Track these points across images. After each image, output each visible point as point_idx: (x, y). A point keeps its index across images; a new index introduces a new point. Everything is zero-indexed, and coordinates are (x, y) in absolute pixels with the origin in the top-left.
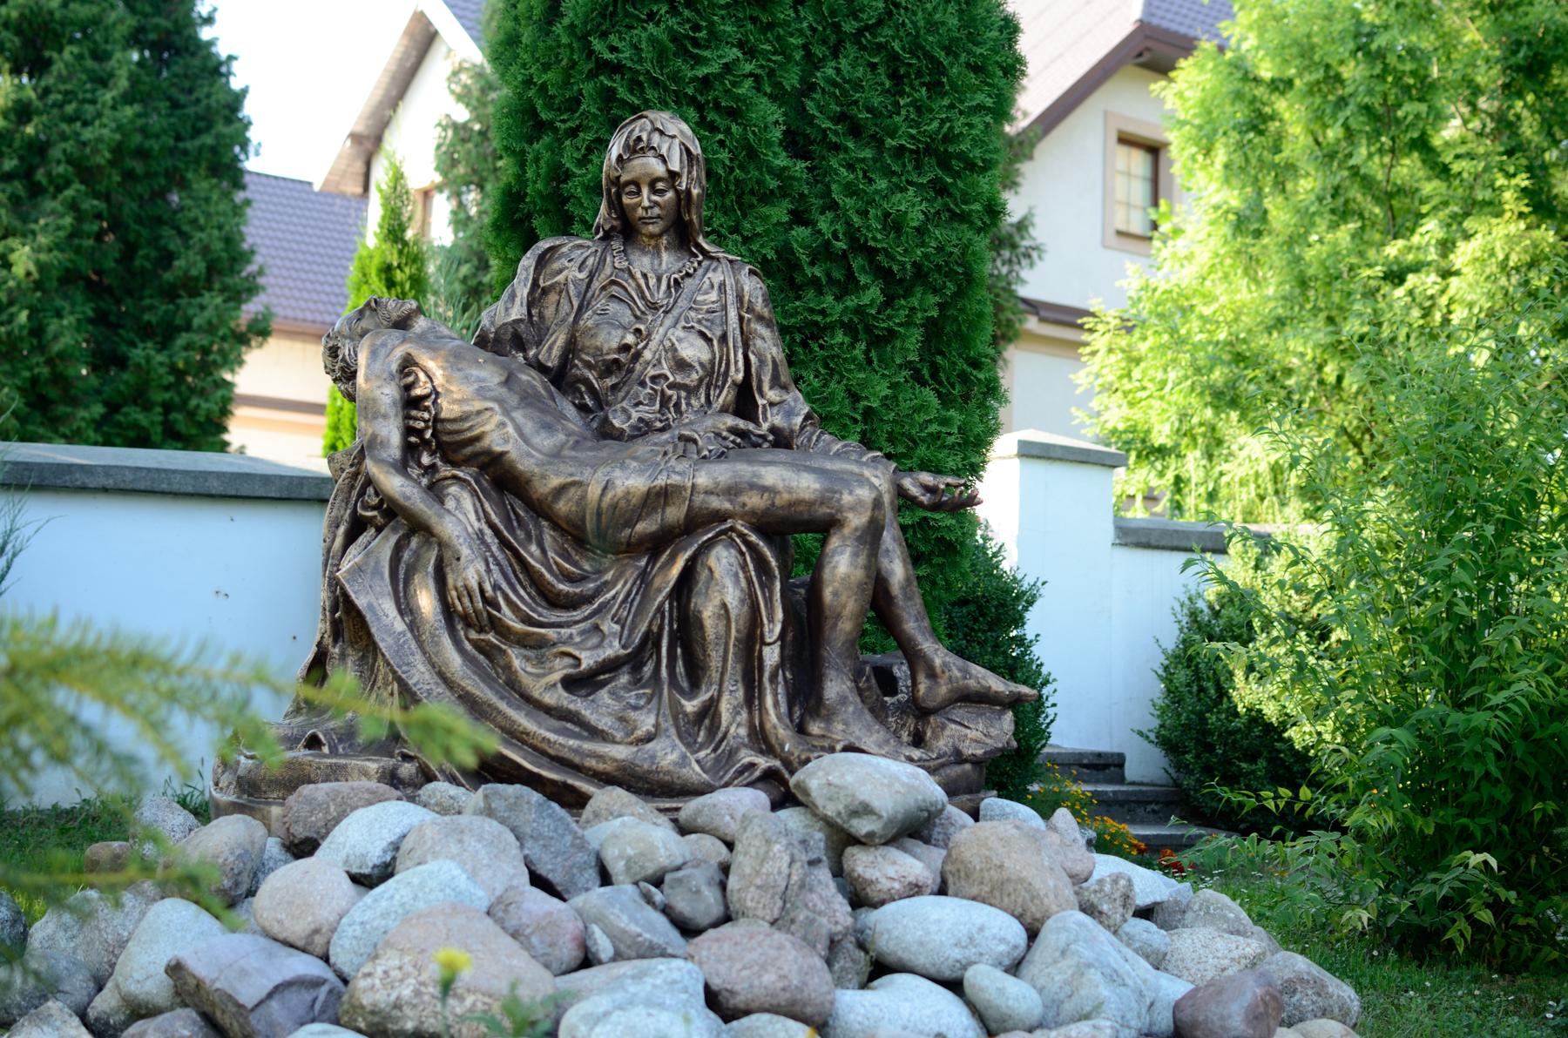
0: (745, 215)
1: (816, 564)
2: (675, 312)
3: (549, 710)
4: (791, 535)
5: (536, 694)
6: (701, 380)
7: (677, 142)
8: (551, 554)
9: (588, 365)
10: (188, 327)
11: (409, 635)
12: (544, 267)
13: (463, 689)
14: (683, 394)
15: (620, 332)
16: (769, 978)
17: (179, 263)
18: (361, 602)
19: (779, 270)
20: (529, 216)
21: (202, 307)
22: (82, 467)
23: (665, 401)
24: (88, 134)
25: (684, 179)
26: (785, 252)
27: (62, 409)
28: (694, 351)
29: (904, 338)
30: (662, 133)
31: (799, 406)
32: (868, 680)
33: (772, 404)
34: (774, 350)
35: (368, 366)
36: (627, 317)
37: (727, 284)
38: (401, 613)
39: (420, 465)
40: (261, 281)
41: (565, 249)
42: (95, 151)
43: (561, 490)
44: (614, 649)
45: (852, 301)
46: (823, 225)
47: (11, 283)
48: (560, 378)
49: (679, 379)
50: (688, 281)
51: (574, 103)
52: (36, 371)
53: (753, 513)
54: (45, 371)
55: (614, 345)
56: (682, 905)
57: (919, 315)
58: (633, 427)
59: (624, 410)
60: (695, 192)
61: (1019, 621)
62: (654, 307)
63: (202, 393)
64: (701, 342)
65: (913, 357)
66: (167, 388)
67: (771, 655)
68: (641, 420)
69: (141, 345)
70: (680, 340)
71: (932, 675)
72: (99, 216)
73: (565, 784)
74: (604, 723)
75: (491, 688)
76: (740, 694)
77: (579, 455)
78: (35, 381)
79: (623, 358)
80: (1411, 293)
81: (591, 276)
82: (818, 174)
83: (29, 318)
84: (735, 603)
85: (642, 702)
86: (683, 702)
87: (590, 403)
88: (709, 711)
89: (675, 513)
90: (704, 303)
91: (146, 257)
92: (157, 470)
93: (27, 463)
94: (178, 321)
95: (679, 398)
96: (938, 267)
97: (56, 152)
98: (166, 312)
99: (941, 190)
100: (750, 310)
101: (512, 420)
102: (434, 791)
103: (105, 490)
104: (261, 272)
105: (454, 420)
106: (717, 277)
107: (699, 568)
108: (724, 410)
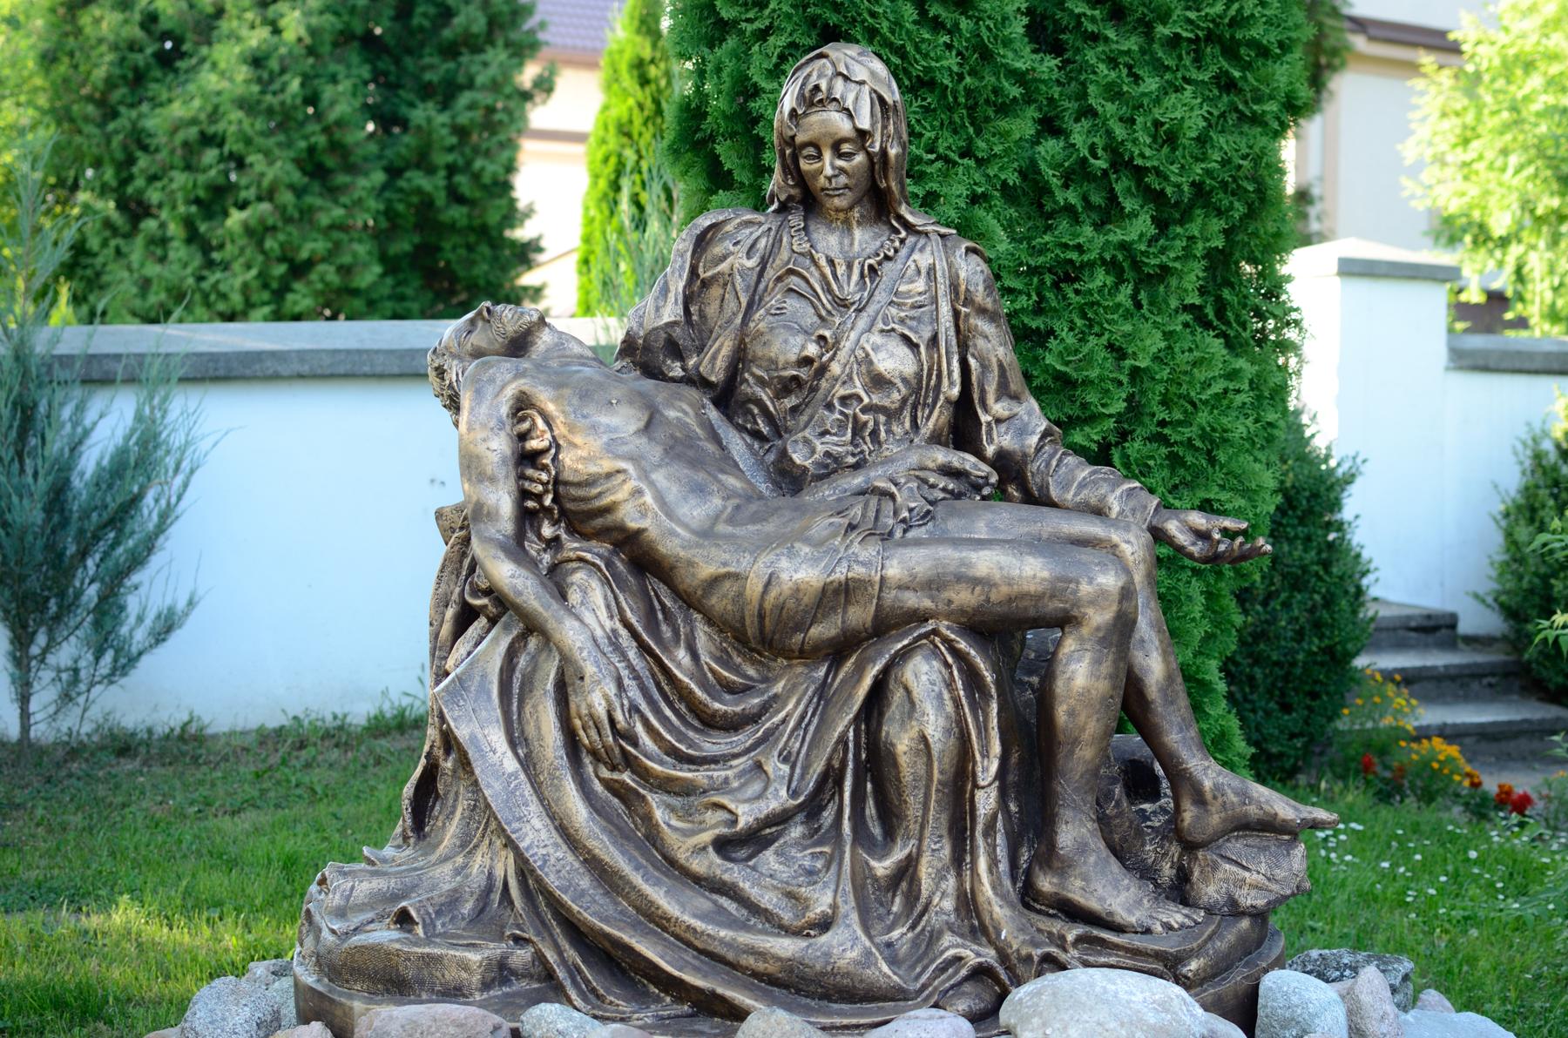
0: (978, 132)
1: (1047, 666)
2: (871, 309)
3: (698, 880)
4: (1010, 639)
5: (682, 856)
6: (904, 401)
7: (866, 89)
8: (705, 658)
9: (761, 382)
10: (470, 85)
11: (522, 776)
12: (704, 250)
13: (589, 851)
14: (882, 418)
15: (800, 339)
17: (459, 21)
18: (462, 732)
19: (1025, 194)
20: (712, 138)
21: (485, 64)
22: (273, 354)
23: (858, 428)
25: (878, 137)
26: (1030, 172)
27: (341, 179)
28: (894, 361)
29: (1180, 275)
30: (846, 78)
31: (1034, 421)
32: (1118, 804)
33: (998, 421)
34: (1001, 351)
35: (472, 409)
36: (810, 318)
37: (936, 267)
38: (513, 744)
39: (540, 536)
40: (541, 36)
41: (729, 228)
43: (715, 581)
44: (778, 799)
45: (1116, 236)
46: (1078, 138)
47: (283, 51)
48: (727, 397)
49: (876, 399)
50: (888, 266)
52: (313, 140)
53: (962, 612)
54: (321, 140)
55: (793, 358)
57: (1200, 245)
58: (818, 464)
59: (806, 441)
60: (893, 152)
61: (1336, 505)
62: (842, 304)
63: (487, 154)
64: (904, 351)
65: (1194, 299)
66: (451, 149)
67: (986, 801)
68: (827, 454)
69: (421, 106)
70: (876, 349)
71: (1200, 800)
73: (713, 993)
74: (768, 899)
75: (623, 853)
76: (946, 852)
77: (738, 531)
78: (312, 150)
79: (804, 373)
81: (763, 264)
82: (1072, 70)
83: (303, 85)
84: (938, 735)
85: (819, 864)
86: (873, 863)
87: (765, 430)
88: (906, 871)
89: (859, 615)
90: (908, 294)
91: (425, 15)
92: (359, 352)
93: (212, 354)
94: (461, 79)
95: (876, 423)
96: (1224, 184)
98: (448, 71)
99: (1227, 84)
100: (968, 301)
101: (652, 484)
102: (540, 1018)
103: (301, 377)
104: (542, 25)
105: (579, 485)
106: (924, 260)
107: (892, 684)
108: (936, 439)
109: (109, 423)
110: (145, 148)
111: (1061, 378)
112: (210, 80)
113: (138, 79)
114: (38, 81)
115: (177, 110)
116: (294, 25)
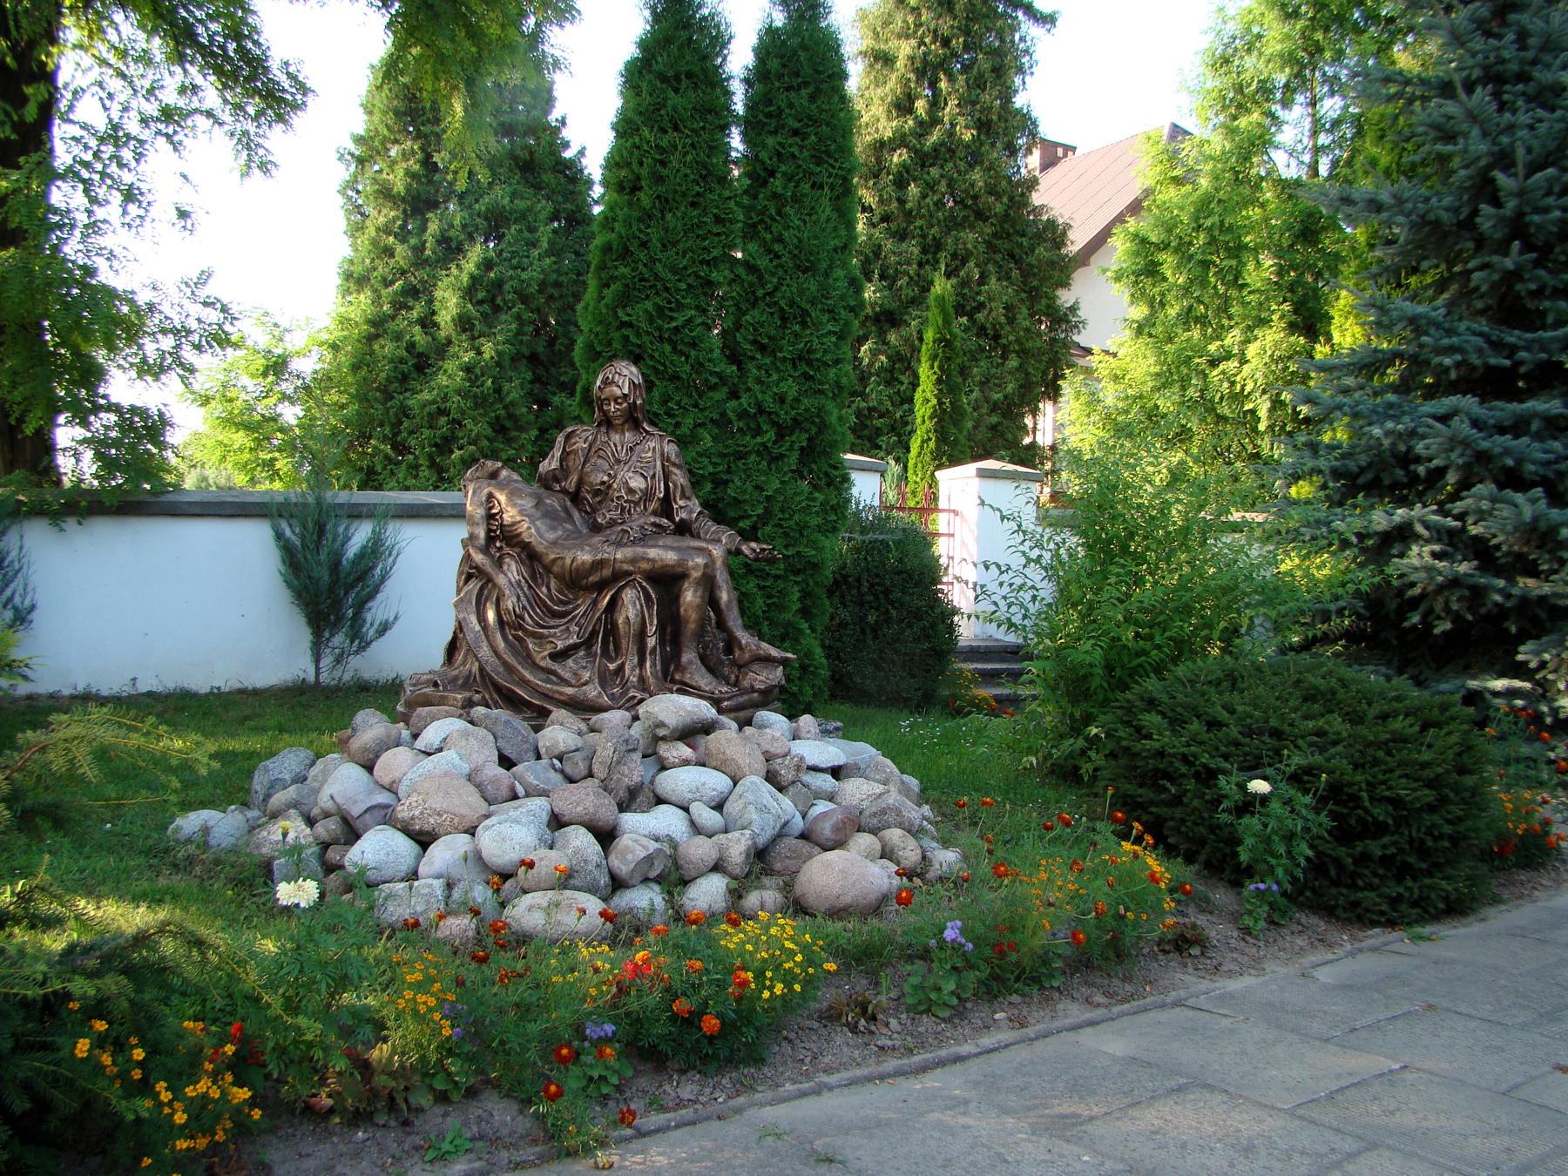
4: (666, 582)
16: (579, 809)
23: (623, 509)
24: (524, 276)
26: (723, 414)
27: (514, 434)
28: (637, 483)
36: (606, 467)
37: (656, 447)
42: (529, 285)
43: (555, 560)
44: (574, 640)
45: (759, 440)
48: (576, 498)
51: (610, 344)
54: (502, 412)
56: (568, 770)
62: (618, 461)
71: (741, 648)
72: (533, 322)
74: (567, 676)
78: (498, 418)
80: (1223, 372)
88: (621, 668)
89: (607, 572)
97: (507, 287)
100: (668, 460)
106: (652, 444)
108: (654, 513)
109: (361, 535)
110: (407, 417)
111: (735, 499)
112: (443, 380)
113: (404, 378)
114: (350, 379)
115: (426, 396)
116: (488, 350)
